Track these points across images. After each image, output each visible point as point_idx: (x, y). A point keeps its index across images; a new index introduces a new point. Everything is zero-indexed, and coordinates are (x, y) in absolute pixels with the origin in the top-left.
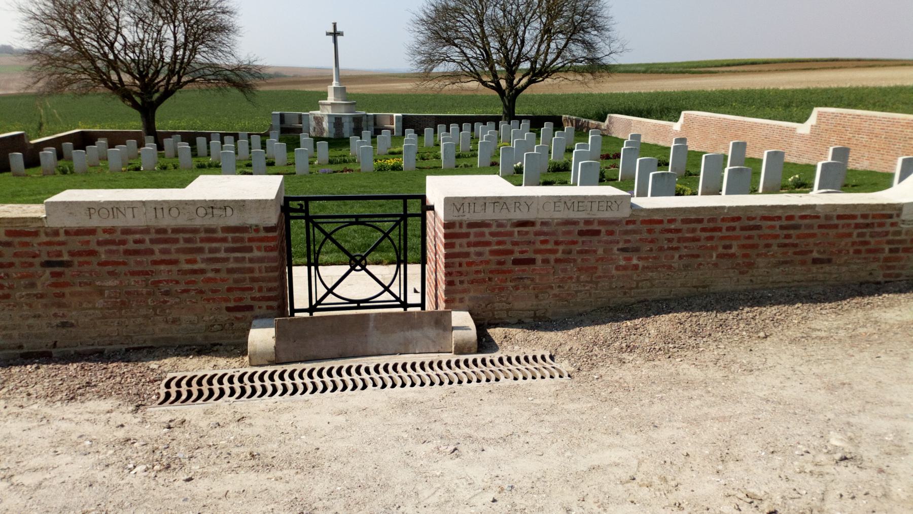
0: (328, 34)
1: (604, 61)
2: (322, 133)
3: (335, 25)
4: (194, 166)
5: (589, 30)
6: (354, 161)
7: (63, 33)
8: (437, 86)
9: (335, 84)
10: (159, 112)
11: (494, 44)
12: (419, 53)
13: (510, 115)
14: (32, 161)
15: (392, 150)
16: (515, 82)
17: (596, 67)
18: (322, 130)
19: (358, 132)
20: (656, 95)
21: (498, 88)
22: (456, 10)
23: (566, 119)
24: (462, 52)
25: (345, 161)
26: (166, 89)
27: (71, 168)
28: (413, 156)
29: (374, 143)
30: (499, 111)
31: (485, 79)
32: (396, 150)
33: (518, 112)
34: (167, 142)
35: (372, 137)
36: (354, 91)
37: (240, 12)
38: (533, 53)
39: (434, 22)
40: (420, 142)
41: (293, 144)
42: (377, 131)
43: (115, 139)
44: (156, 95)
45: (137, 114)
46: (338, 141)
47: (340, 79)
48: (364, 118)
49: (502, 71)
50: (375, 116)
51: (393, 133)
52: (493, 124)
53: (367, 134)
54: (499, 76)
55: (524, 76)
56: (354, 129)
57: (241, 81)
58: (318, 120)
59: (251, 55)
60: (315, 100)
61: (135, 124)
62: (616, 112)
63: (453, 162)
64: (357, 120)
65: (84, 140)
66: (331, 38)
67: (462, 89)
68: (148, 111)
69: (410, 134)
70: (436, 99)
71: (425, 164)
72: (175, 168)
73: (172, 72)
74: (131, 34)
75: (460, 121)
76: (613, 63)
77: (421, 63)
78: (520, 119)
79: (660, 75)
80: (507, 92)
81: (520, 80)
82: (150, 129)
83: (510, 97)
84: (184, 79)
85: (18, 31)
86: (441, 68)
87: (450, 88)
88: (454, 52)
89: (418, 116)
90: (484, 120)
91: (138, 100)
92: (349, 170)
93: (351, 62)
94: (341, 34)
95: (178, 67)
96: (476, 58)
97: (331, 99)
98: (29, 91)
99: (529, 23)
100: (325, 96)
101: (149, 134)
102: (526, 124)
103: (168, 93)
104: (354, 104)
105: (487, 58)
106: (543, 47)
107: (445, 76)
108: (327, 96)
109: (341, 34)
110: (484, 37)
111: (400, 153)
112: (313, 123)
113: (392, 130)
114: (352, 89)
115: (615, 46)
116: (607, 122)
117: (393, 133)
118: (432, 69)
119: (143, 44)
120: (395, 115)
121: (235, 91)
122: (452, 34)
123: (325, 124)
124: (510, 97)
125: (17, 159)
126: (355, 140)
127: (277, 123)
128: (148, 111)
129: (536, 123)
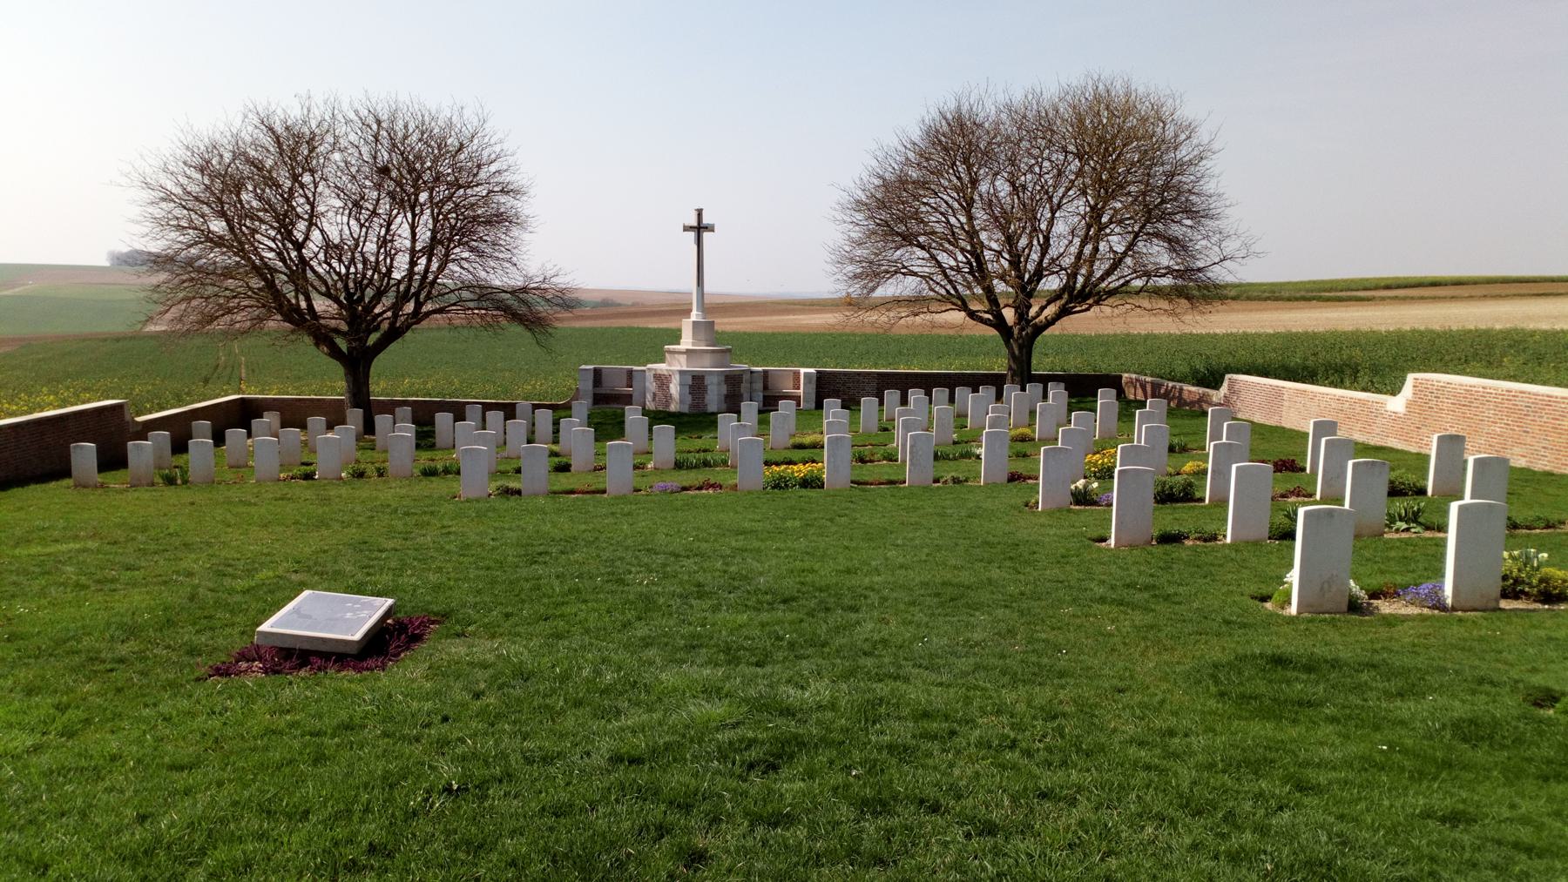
0: (687, 229)
1: (1209, 274)
2: (667, 404)
3: (700, 213)
4: (417, 472)
5: (1178, 217)
6: (725, 463)
7: (218, 226)
8: (884, 318)
9: (695, 315)
10: (380, 363)
11: (991, 240)
12: (852, 260)
13: (1023, 375)
14: (113, 460)
15: (798, 440)
16: (1033, 311)
17: (1194, 289)
18: (668, 398)
19: (733, 404)
20: (1356, 339)
21: (999, 323)
22: (923, 184)
23: (1131, 381)
24: (933, 257)
25: (706, 464)
26: (392, 324)
27: (184, 472)
28: (847, 454)
29: (763, 422)
30: (1000, 365)
31: (974, 306)
32: (807, 440)
33: (1040, 365)
34: (382, 421)
35: (760, 412)
36: (728, 328)
37: (532, 192)
38: (1067, 261)
39: (882, 204)
40: (854, 422)
41: (608, 424)
42: (770, 402)
43: (294, 415)
44: (373, 338)
45: (337, 370)
46: (695, 421)
47: (705, 308)
48: (746, 377)
49: (1007, 294)
50: (765, 372)
51: (798, 404)
52: (992, 390)
53: (750, 408)
54: (1002, 302)
55: (1049, 303)
56: (727, 397)
57: (526, 312)
58: (662, 380)
59: (549, 266)
60: (658, 343)
61: (333, 384)
62: (1239, 371)
63: (929, 469)
64: (733, 380)
65: (244, 414)
66: (692, 235)
67: (933, 325)
68: (357, 364)
69: (832, 407)
70: (881, 342)
71: (867, 472)
72: (381, 475)
73: (403, 298)
74: (336, 224)
75: (927, 383)
76: (1230, 279)
77: (856, 276)
78: (1044, 380)
79: (1264, 304)
80: (1016, 331)
81: (1042, 309)
82: (360, 394)
83: (1022, 339)
84: (428, 307)
85: (138, 222)
86: (888, 289)
87: (911, 323)
88: (916, 258)
89: (845, 374)
90: (974, 382)
91: (343, 344)
92: (713, 486)
93: (723, 282)
94: (710, 228)
95: (421, 289)
96: (959, 270)
97: (687, 342)
98: (151, 328)
99: (1059, 206)
100: (676, 337)
101: (356, 405)
102: (1057, 392)
103: (394, 334)
104: (729, 351)
105: (979, 271)
106: (1088, 249)
107: (897, 301)
108: (680, 337)
109: (710, 228)
110: (972, 234)
111: (817, 446)
112: (651, 386)
113: (797, 399)
114: (725, 324)
115: (1230, 246)
116: (1224, 389)
117: (798, 404)
118: (873, 289)
119: (357, 245)
120: (803, 371)
121: (517, 329)
122: (914, 226)
123: (674, 389)
124: (1022, 339)
125: (85, 454)
126: (727, 422)
127: (588, 385)
128: (357, 364)
129: (1081, 389)
